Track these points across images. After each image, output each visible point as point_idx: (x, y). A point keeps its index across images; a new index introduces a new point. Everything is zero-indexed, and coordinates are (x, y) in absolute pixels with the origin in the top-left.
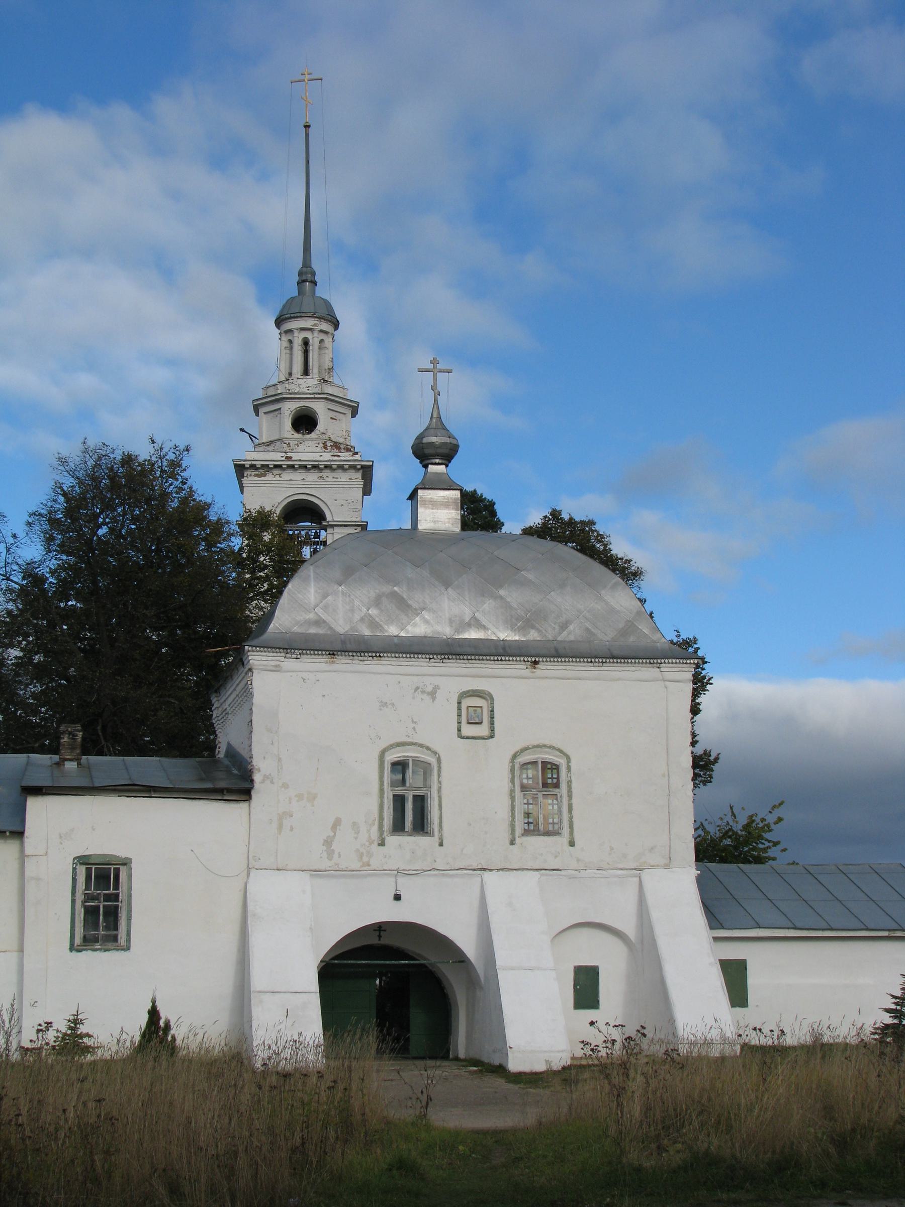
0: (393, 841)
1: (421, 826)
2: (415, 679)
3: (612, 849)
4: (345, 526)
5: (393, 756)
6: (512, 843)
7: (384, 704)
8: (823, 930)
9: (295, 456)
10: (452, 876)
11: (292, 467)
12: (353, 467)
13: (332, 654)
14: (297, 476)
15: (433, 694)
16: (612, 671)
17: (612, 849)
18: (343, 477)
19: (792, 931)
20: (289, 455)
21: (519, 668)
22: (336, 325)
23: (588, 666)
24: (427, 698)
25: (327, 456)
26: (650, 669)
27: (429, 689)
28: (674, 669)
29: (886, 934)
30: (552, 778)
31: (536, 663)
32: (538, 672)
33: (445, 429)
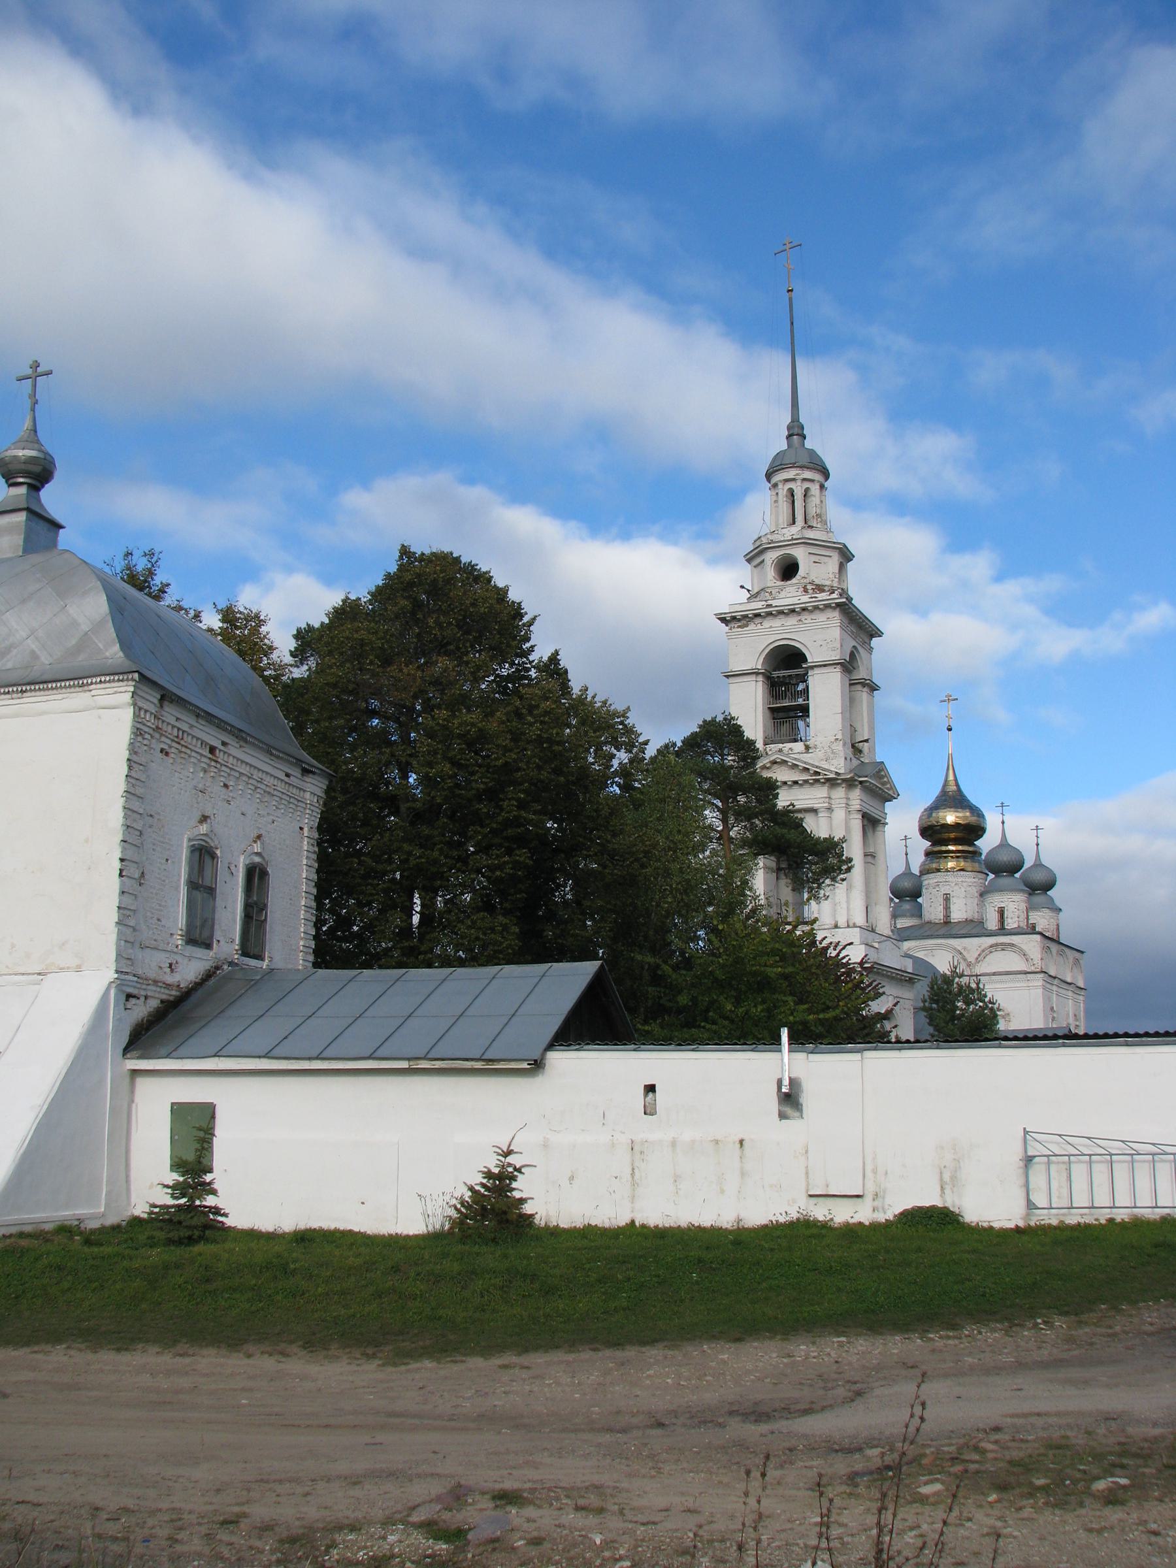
3: (13, 946)
4: (825, 666)
8: (310, 1059)
9: (774, 603)
11: (770, 614)
12: (827, 606)
14: (776, 623)
18: (821, 617)
19: (371, 1061)
20: (770, 602)
22: (826, 474)
25: (805, 598)
26: (82, 694)
28: (109, 691)
29: (404, 1065)
33: (38, 442)
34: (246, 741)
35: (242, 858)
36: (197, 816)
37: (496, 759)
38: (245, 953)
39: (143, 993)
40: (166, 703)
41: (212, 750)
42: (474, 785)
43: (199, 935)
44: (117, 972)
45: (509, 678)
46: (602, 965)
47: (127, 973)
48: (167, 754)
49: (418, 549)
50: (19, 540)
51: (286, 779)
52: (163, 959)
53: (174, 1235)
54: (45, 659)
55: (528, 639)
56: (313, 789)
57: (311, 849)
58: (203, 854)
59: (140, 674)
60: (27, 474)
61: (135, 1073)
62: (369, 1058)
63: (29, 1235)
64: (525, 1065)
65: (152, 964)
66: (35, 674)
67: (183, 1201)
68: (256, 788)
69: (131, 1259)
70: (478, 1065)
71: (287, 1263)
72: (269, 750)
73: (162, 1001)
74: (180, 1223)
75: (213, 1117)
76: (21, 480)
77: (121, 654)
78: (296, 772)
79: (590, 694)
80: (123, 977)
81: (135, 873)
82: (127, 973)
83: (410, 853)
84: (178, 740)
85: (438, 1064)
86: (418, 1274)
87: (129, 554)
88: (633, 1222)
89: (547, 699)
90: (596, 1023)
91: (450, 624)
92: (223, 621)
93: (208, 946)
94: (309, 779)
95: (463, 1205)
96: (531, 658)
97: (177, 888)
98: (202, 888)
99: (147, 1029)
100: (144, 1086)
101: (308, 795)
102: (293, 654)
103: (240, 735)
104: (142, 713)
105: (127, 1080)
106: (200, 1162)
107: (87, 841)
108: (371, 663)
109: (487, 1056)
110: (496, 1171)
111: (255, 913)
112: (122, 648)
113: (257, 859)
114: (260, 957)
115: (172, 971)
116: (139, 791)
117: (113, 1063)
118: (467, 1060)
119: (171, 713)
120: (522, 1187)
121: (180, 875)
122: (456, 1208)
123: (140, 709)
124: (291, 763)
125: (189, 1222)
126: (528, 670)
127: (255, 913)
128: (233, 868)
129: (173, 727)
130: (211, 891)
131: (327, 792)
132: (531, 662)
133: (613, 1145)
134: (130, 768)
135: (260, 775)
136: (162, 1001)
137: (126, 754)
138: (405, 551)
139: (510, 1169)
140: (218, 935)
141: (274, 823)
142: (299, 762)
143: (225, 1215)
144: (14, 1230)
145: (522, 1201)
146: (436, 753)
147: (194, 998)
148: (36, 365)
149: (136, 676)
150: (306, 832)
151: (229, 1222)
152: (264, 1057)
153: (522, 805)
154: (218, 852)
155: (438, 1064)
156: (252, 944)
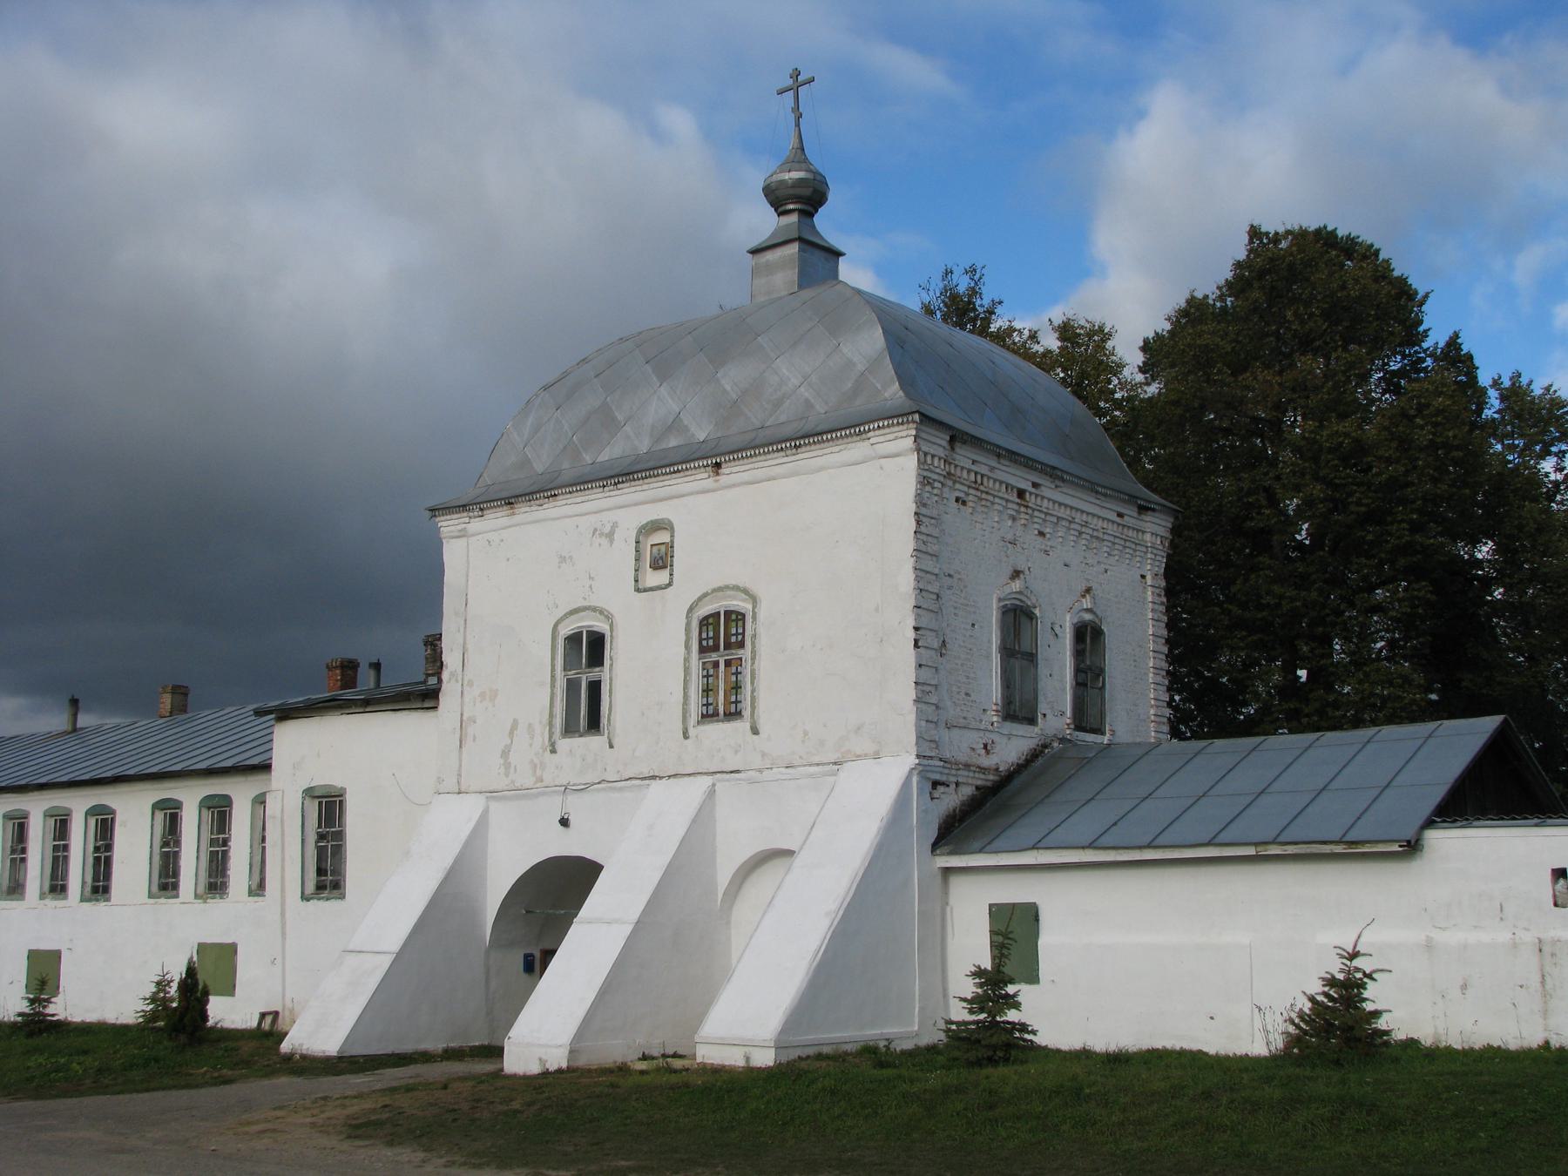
0: (565, 744)
1: (594, 724)
2: (592, 518)
3: (806, 733)
5: (566, 630)
6: (686, 736)
7: (563, 559)
8: (1140, 848)
10: (621, 789)
13: (510, 502)
15: (610, 536)
16: (811, 458)
17: (806, 733)
21: (700, 479)
23: (779, 458)
24: (604, 541)
26: (861, 444)
27: (607, 529)
29: (1251, 851)
30: (737, 634)
31: (718, 465)
32: (724, 479)
33: (806, 160)
34: (1063, 481)
35: (1068, 617)
36: (1009, 571)
37: (1378, 474)
38: (1079, 727)
39: (953, 779)
40: (958, 445)
41: (1021, 494)
42: (1353, 508)
43: (1019, 709)
44: (918, 756)
45: (1401, 373)
46: (1505, 720)
47: (931, 758)
48: (964, 503)
49: (1270, 226)
50: (792, 274)
51: (1118, 520)
52: (976, 739)
53: (972, 1056)
54: (820, 408)
55: (1420, 322)
56: (1155, 530)
57: (1157, 600)
58: (1018, 617)
59: (921, 414)
60: (797, 199)
61: (947, 872)
62: (1209, 844)
63: (827, 1057)
64: (1395, 848)
65: (962, 745)
66: (808, 428)
67: (982, 1016)
68: (1081, 533)
69: (912, 1082)
70: (1339, 849)
71: (1081, 1089)
72: (1092, 488)
73: (977, 788)
74: (978, 1041)
75: (1037, 919)
76: (791, 207)
77: (901, 393)
78: (1130, 511)
79: (1524, 381)
80: (925, 762)
81: (933, 641)
82: (931, 758)
83: (1281, 597)
84: (976, 486)
85: (1291, 849)
86: (1232, 1102)
87: (948, 273)
88: (1547, 1042)
89: (1440, 394)
90: (1490, 793)
91: (1311, 315)
92: (1062, 338)
93: (1032, 721)
94: (1148, 517)
95: (1303, 1019)
96: (1425, 345)
97: (988, 656)
98: (1018, 653)
99: (961, 820)
100: (958, 885)
101: (1148, 537)
102: (1142, 370)
103: (1053, 473)
104: (929, 458)
105: (939, 878)
106: (999, 971)
107: (877, 610)
108: (1220, 372)
109: (1350, 837)
110: (1341, 976)
111: (1089, 676)
112: (902, 387)
113: (1088, 617)
114: (1099, 731)
115: (988, 752)
116: (933, 548)
117: (920, 863)
118: (1324, 843)
119: (964, 457)
120: (1374, 996)
121: (990, 641)
122: (1293, 1022)
123: (926, 454)
124: (1124, 501)
125: (991, 1041)
126: (1424, 360)
127: (1089, 676)
128: (1057, 629)
129: (969, 471)
130: (1031, 657)
131: (1173, 530)
132: (1425, 351)
133: (1515, 946)
134: (918, 523)
135: (1084, 517)
136: (977, 788)
137: (913, 507)
138: (1254, 233)
139: (1359, 975)
140: (1043, 707)
141: (1109, 574)
142: (1132, 499)
143: (1034, 1032)
144: (811, 1051)
145: (1376, 1014)
146: (1303, 475)
147: (1016, 783)
148: (796, 74)
149: (917, 417)
150: (1149, 580)
151: (1042, 1039)
152: (1033, 848)
153: (1415, 528)
154: (1037, 612)
155: (1291, 849)
156: (1087, 716)
